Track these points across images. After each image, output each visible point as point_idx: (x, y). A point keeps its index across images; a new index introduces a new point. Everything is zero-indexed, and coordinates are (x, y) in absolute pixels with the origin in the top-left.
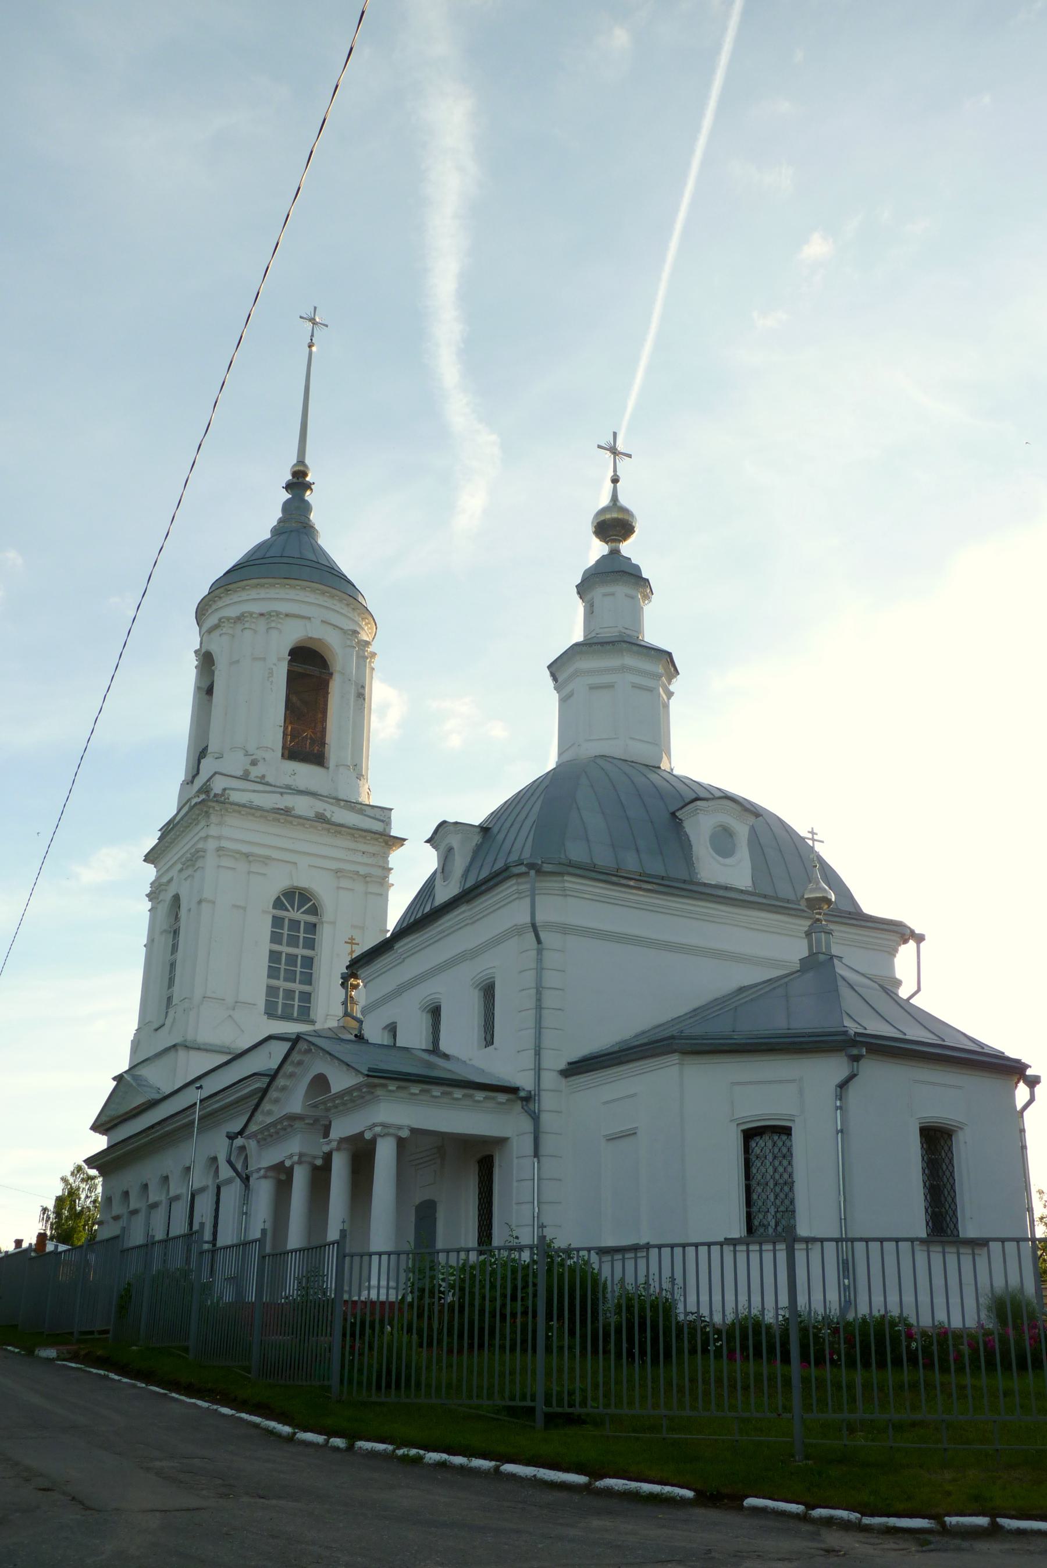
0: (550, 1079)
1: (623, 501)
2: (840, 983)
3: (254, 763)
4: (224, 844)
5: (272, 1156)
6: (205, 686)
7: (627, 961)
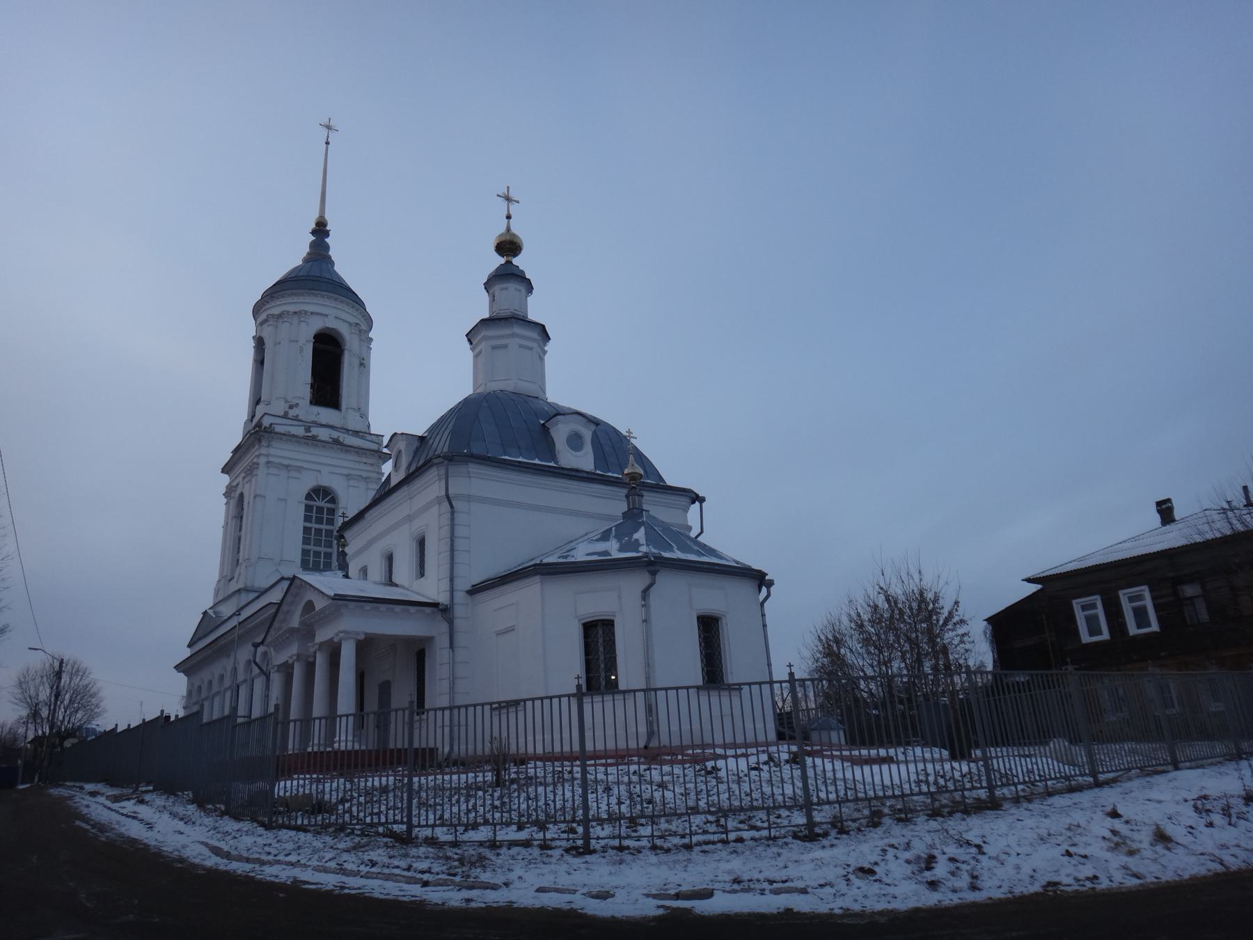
0: (460, 597)
1: (514, 230)
3: (291, 407)
4: (271, 459)
5: (280, 658)
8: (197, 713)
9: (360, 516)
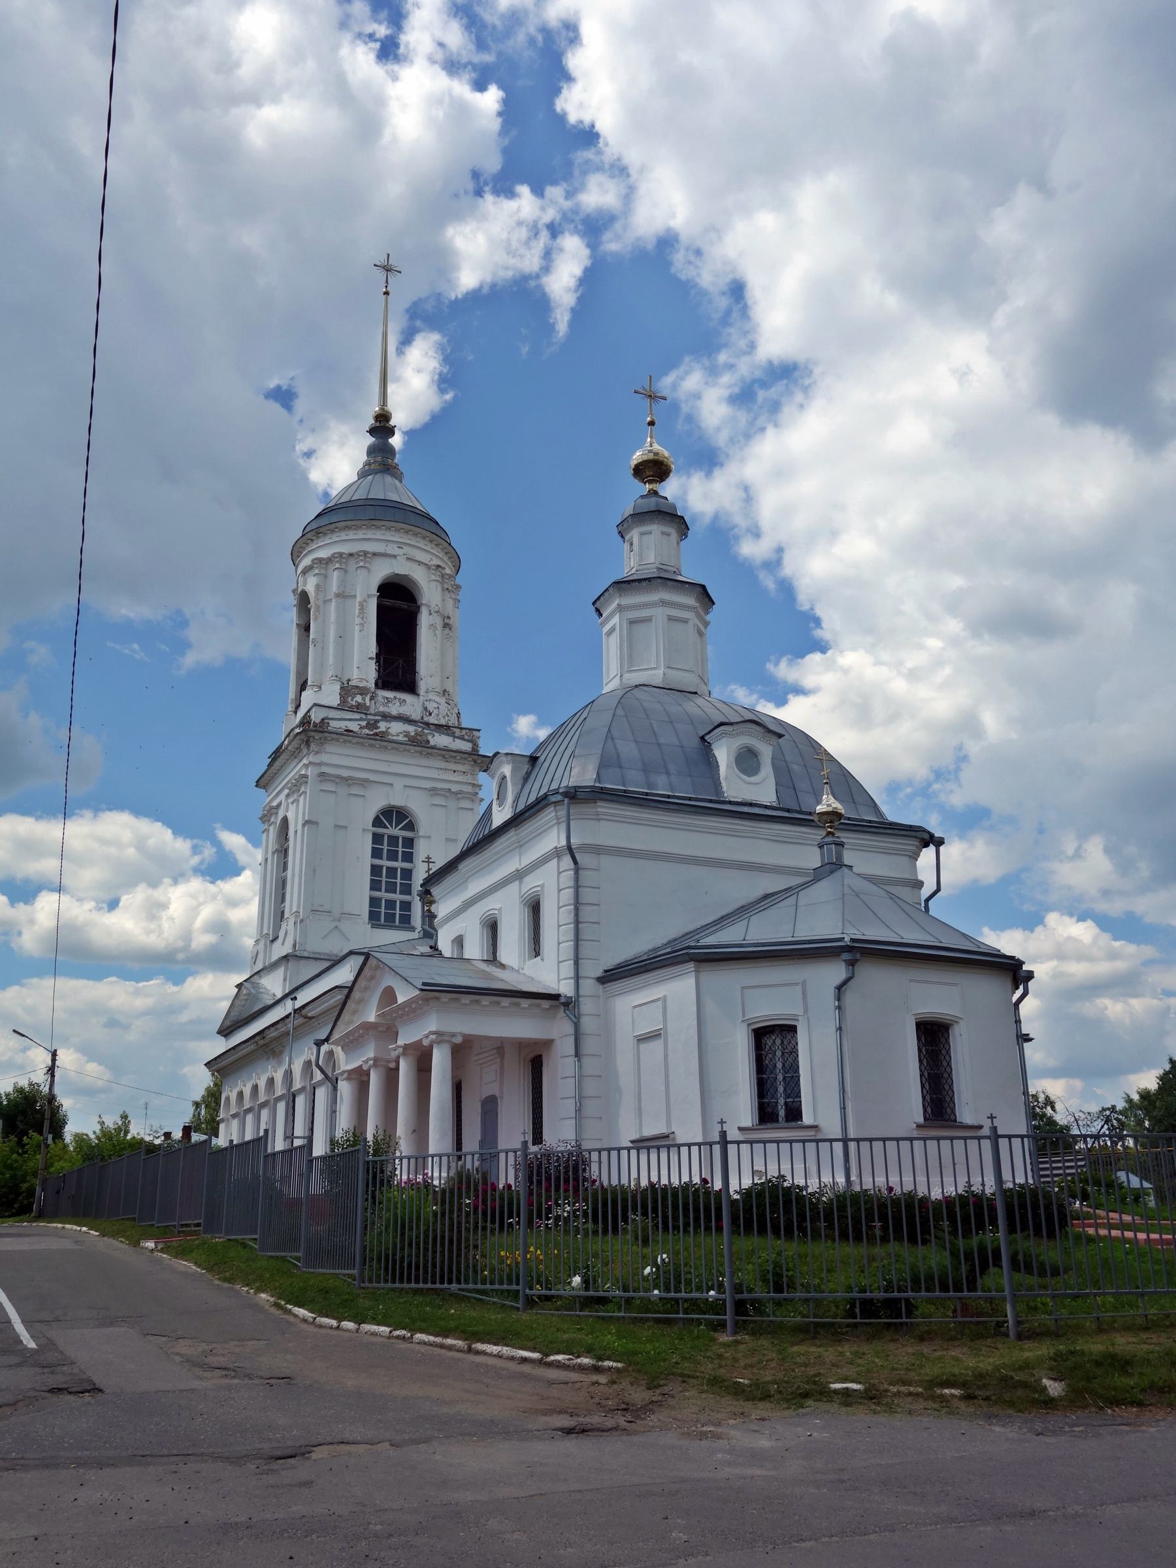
4: (325, 769)
5: (345, 1063)
9: (451, 867)
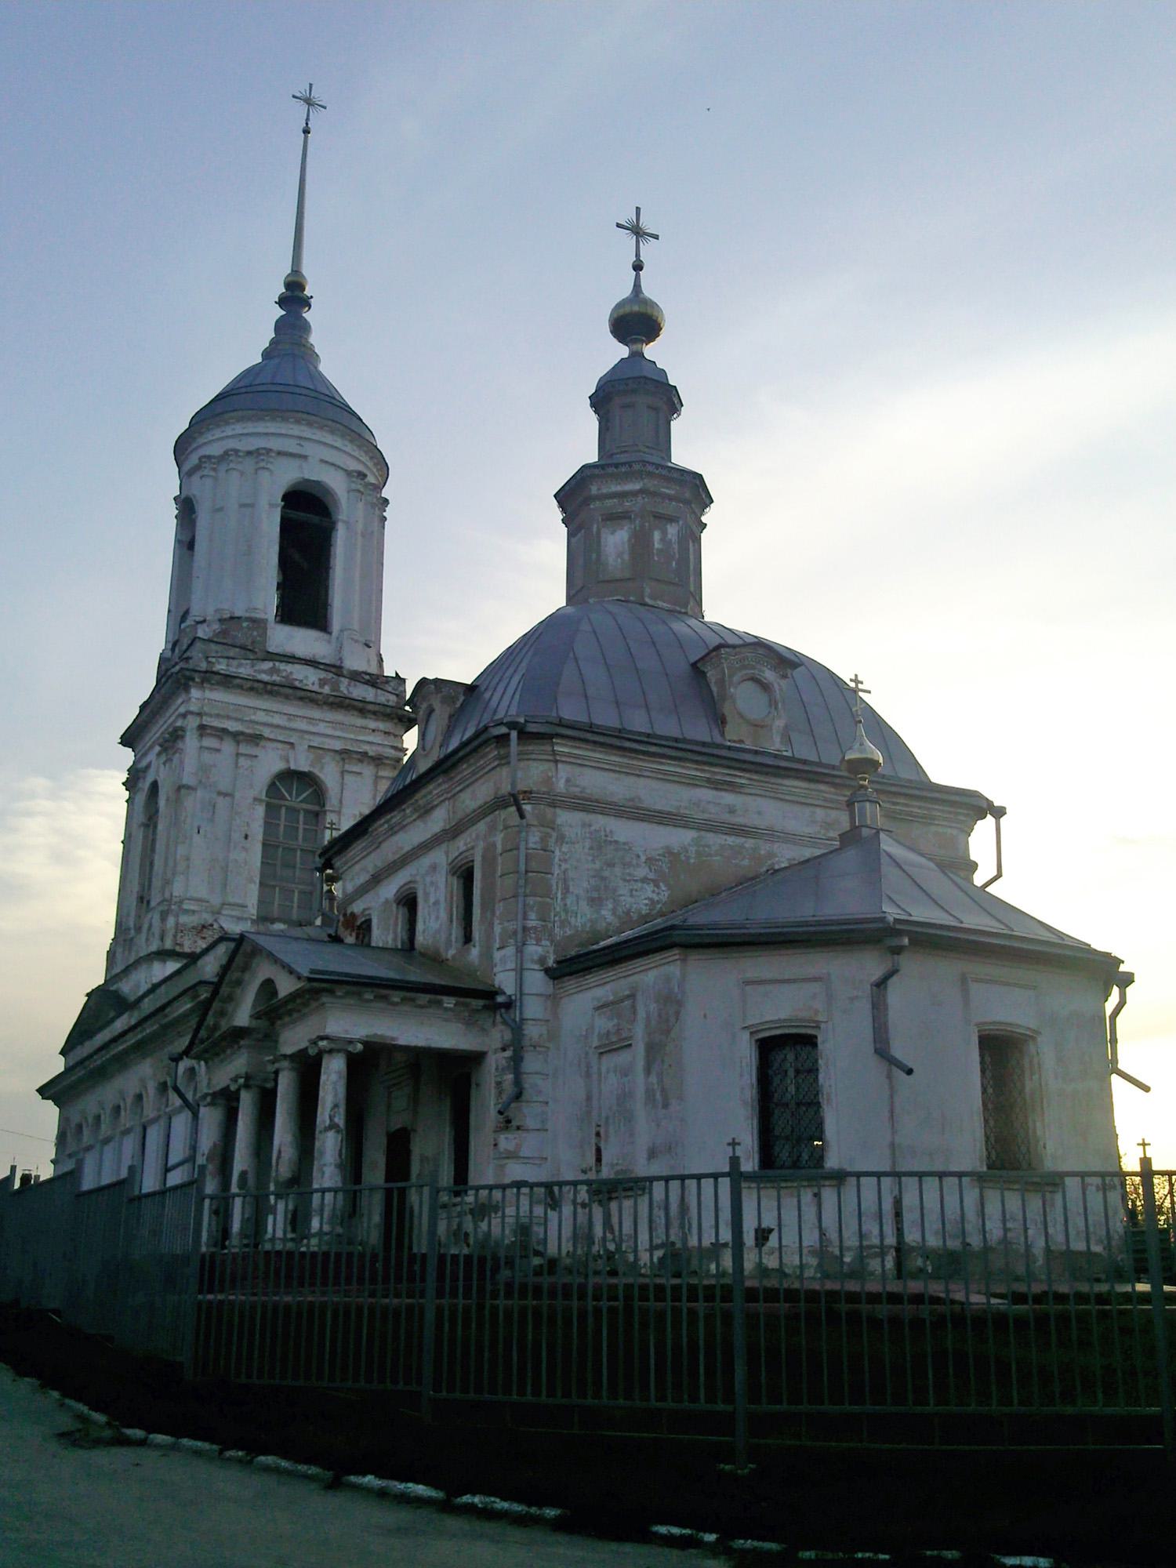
1: (648, 291)
2: (884, 859)
4: (206, 720)
6: (186, 538)
7: (619, 840)
8: (71, 1173)
9: (361, 829)
